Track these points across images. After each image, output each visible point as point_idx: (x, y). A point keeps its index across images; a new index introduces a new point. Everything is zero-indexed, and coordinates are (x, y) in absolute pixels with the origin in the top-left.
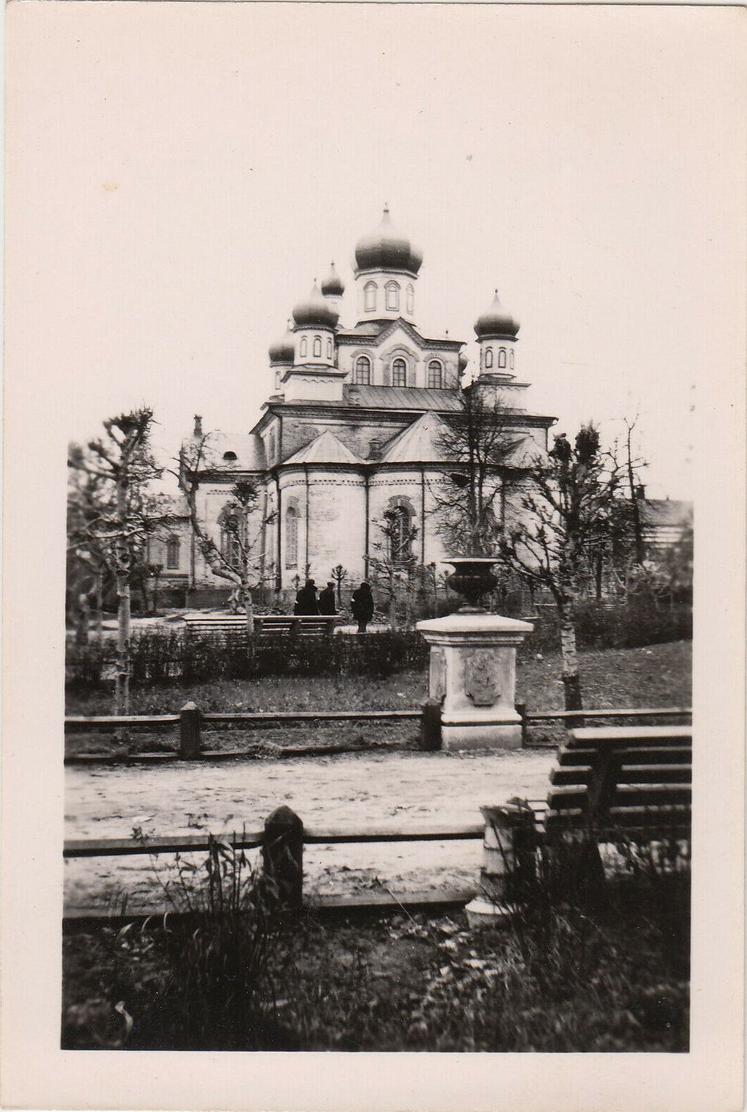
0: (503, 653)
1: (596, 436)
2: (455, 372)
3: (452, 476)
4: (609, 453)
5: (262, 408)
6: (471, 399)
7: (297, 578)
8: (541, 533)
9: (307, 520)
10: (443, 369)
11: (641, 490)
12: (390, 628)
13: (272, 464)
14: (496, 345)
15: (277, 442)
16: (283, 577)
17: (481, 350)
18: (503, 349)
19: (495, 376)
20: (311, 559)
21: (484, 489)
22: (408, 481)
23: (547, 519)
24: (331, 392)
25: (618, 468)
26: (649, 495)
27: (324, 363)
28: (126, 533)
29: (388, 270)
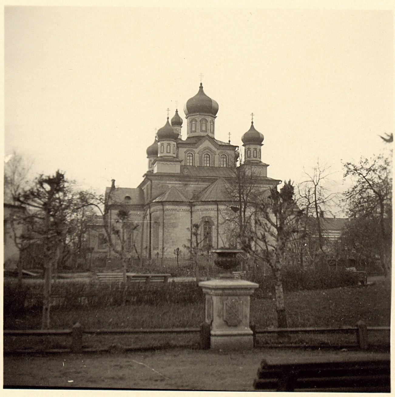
0: (243, 298)
1: (292, 188)
2: (233, 160)
3: (231, 207)
4: (306, 197)
5: (143, 176)
6: (240, 172)
7: (158, 254)
8: (264, 237)
9: (163, 228)
10: (227, 158)
11: (322, 213)
12: (195, 280)
13: (147, 202)
14: (252, 147)
15: (149, 192)
16: (152, 254)
17: (168, 118)
18: (256, 149)
19: (252, 161)
20: (165, 245)
21: (246, 213)
22: (211, 210)
23: (267, 229)
24: (176, 169)
25: (310, 203)
26: (325, 216)
27: (171, 155)
28: (49, 236)
29: (202, 114)
